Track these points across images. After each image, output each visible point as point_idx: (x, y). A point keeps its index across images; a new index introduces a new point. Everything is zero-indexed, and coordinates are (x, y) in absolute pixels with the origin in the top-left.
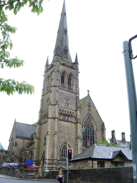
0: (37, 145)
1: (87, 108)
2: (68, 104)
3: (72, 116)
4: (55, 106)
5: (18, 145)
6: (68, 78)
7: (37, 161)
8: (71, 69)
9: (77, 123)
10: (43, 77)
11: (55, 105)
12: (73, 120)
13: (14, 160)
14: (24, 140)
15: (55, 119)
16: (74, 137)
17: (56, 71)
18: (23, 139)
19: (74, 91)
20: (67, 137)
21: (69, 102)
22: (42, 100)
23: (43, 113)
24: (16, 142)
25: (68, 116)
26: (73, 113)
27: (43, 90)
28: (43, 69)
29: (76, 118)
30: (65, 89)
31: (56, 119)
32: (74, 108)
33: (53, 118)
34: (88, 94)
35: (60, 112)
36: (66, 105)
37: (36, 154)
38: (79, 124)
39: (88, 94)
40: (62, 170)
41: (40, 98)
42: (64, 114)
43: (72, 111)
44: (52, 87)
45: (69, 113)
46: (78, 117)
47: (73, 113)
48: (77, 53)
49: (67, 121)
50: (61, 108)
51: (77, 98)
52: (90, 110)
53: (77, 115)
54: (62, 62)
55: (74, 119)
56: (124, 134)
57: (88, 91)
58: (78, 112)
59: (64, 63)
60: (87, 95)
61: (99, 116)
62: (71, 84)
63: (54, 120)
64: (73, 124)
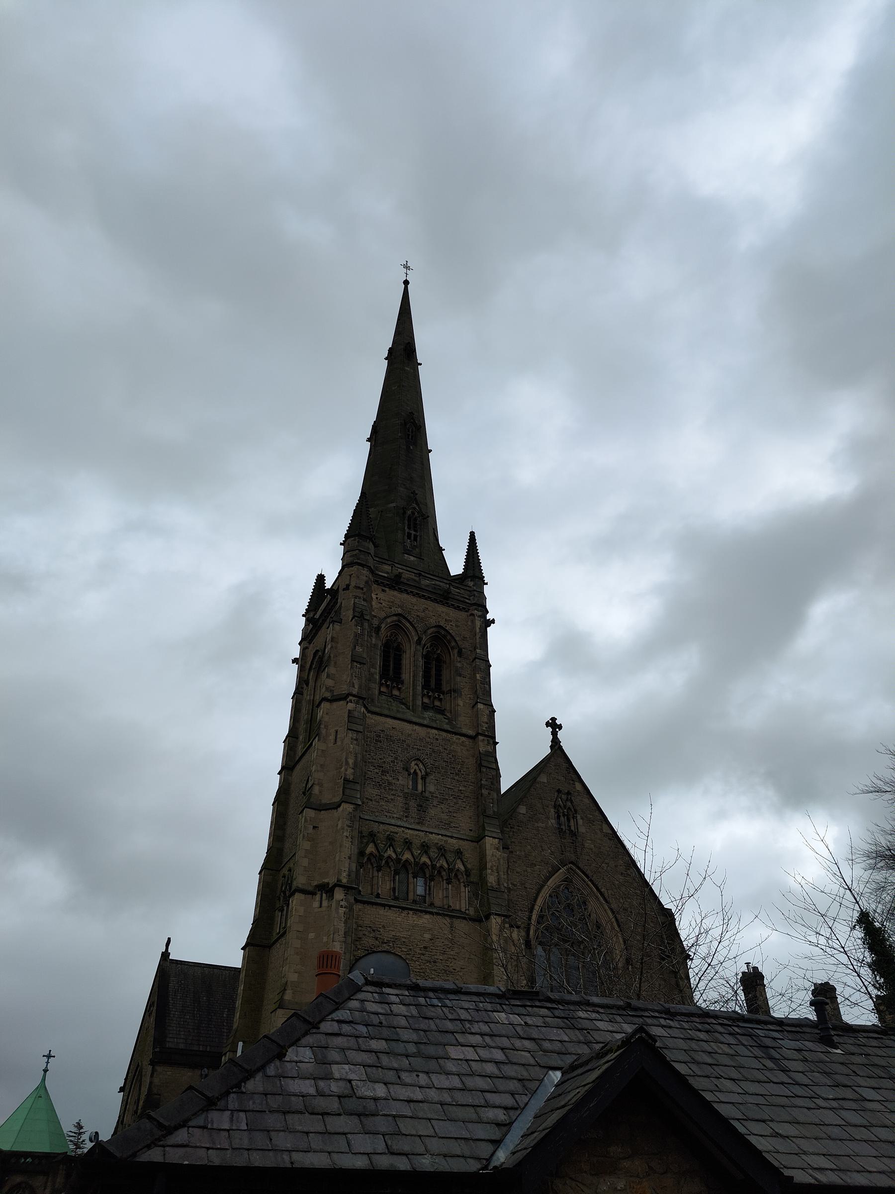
1: (552, 822)
3: (452, 876)
6: (426, 657)
8: (441, 609)
9: (487, 917)
10: (295, 666)
12: (462, 899)
17: (350, 614)
19: (464, 724)
21: (431, 788)
25: (429, 873)
30: (409, 715)
31: (339, 894)
32: (465, 822)
34: (556, 744)
35: (371, 848)
36: (413, 804)
38: (495, 922)
39: (556, 744)
42: (398, 860)
44: (325, 705)
45: (433, 853)
46: (492, 879)
49: (422, 906)
50: (375, 827)
52: (574, 834)
53: (482, 867)
54: (387, 568)
55: (465, 892)
57: (554, 725)
58: (490, 843)
59: (399, 576)
60: (545, 750)
62: (445, 688)
64: (462, 926)
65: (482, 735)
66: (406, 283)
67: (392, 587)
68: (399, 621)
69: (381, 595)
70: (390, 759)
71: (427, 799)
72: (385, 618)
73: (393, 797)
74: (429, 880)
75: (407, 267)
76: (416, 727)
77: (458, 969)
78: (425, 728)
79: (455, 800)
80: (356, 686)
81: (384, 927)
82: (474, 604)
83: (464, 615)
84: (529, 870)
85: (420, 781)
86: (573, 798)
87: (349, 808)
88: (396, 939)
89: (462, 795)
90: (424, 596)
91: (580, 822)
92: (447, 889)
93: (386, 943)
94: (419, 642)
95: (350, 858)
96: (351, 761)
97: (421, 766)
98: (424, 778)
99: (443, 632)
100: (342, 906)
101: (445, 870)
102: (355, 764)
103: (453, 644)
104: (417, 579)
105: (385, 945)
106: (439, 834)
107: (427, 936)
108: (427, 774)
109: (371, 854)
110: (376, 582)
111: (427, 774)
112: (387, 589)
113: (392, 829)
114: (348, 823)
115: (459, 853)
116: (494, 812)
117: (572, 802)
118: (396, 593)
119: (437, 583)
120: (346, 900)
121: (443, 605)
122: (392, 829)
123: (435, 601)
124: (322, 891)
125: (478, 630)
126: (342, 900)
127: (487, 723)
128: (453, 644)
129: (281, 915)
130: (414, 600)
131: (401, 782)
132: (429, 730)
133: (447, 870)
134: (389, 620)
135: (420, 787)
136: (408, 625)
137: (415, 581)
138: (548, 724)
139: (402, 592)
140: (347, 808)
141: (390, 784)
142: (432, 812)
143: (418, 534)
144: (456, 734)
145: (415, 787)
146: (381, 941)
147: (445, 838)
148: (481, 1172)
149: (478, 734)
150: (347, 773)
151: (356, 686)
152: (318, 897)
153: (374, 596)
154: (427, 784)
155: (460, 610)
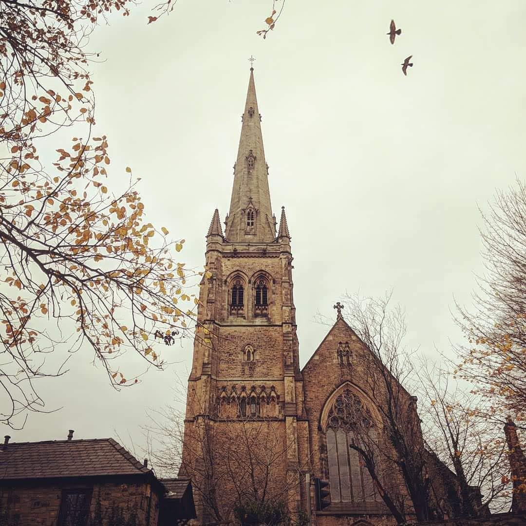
8: (263, 260)
36: (246, 367)
50: (225, 384)
65: (284, 323)
66: (252, 69)
67: (233, 257)
68: (238, 274)
69: (228, 263)
70: (233, 347)
71: (255, 363)
72: (230, 274)
73: (235, 367)
75: (252, 60)
76: (248, 328)
78: (253, 327)
79: (271, 361)
80: (209, 315)
82: (282, 252)
83: (277, 260)
84: (320, 389)
86: (350, 345)
87: (204, 378)
89: (275, 358)
90: (252, 256)
94: (250, 282)
96: (207, 354)
97: (251, 347)
98: (253, 353)
99: (264, 273)
102: (209, 355)
103: (270, 277)
104: (247, 248)
106: (261, 380)
108: (255, 351)
109: (224, 397)
110: (224, 257)
111: (255, 351)
112: (520, 277)
113: (235, 383)
115: (273, 388)
116: (291, 363)
117: (348, 347)
118: (235, 259)
119: (260, 247)
121: (264, 258)
122: (235, 383)
123: (258, 257)
125: (283, 266)
127: (288, 316)
128: (270, 277)
130: (246, 260)
131: (240, 358)
132: (255, 327)
134: (232, 275)
135: (252, 358)
136: (243, 274)
137: (246, 249)
138: (335, 307)
139: (239, 258)
141: (233, 360)
142: (257, 369)
143: (254, 221)
144: (271, 326)
145: (249, 359)
147: (265, 382)
149: (283, 323)
151: (209, 315)
153: (223, 265)
155: (274, 258)
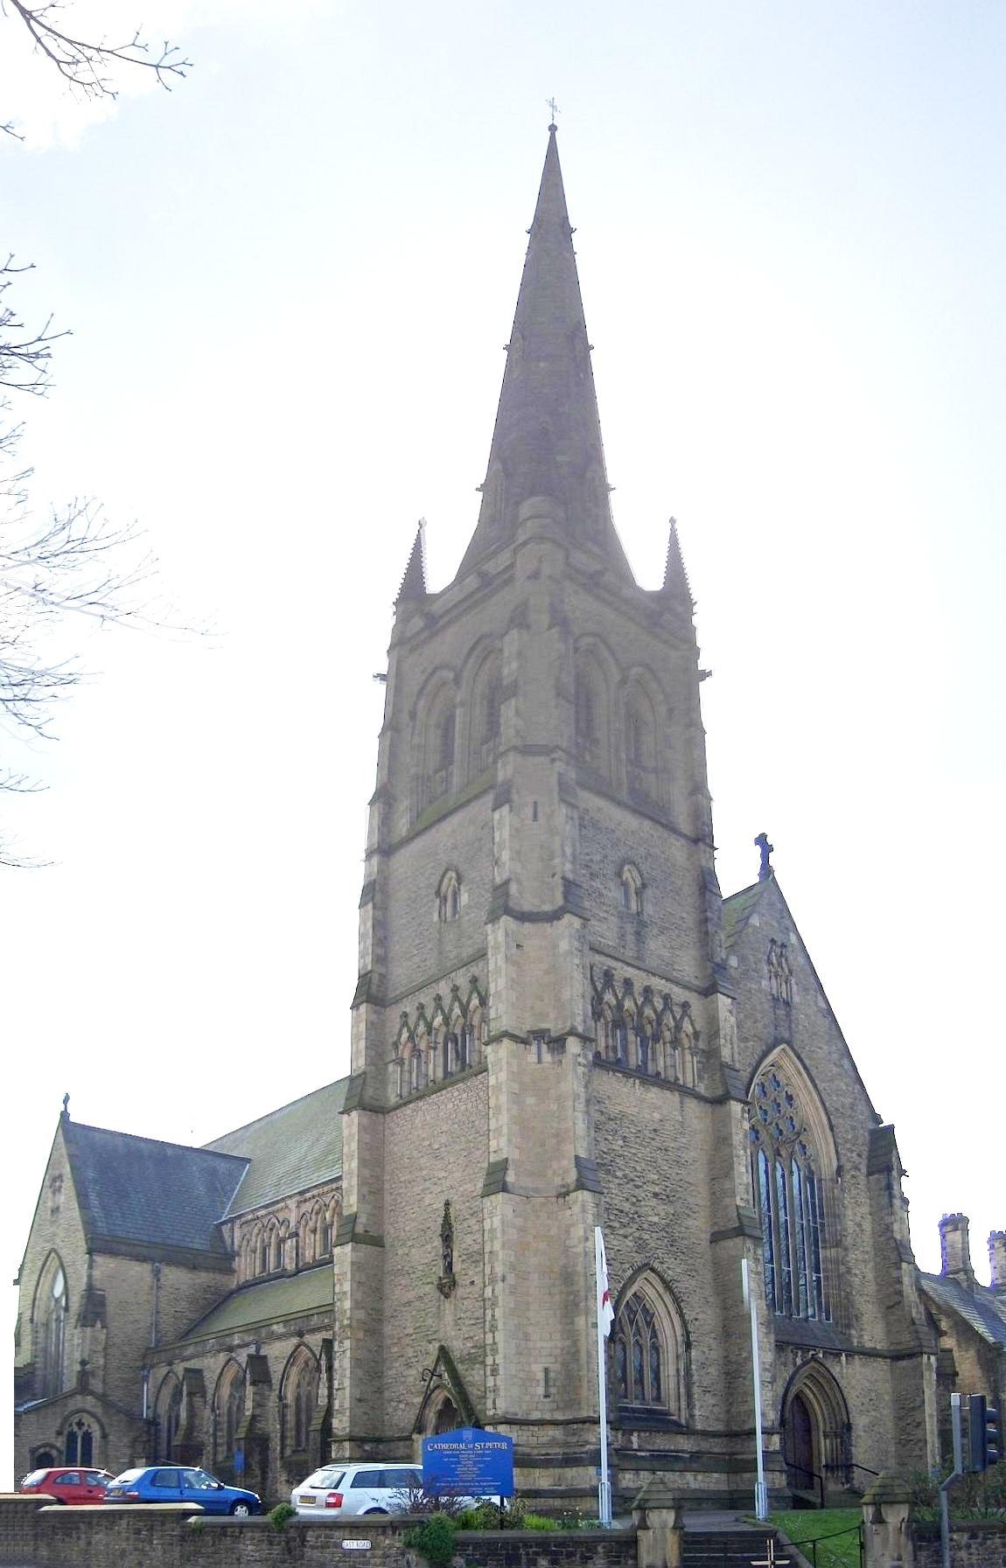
0: (359, 1296)
2: (640, 925)
4: (546, 927)
5: (111, 1309)
7: (363, 1440)
10: (381, 688)
11: (554, 916)
13: (96, 1434)
14: (157, 1273)
15: (557, 1044)
16: (698, 1226)
18: (147, 1267)
20: (655, 1213)
21: (649, 909)
22: (375, 894)
23: (394, 1014)
24: (90, 1288)
26: (685, 1006)
27: (384, 798)
28: (381, 624)
29: (710, 1055)
31: (573, 1045)
32: (688, 965)
33: (539, 1035)
34: (766, 870)
36: (630, 928)
37: (357, 1382)
39: (766, 870)
40: (911, 1520)
41: (354, 873)
43: (679, 994)
45: (658, 1003)
47: (685, 1006)
48: (672, 521)
51: (707, 882)
52: (787, 1004)
53: (714, 1034)
56: (966, 1232)
57: (766, 848)
61: (846, 1062)
63: (547, 1057)
64: (692, 1105)
73: (605, 915)
74: (653, 1040)
77: (690, 1161)
81: (609, 1097)
85: (633, 897)
88: (623, 1115)
91: (795, 988)
92: (673, 1056)
93: (612, 1120)
95: (583, 997)
96: (568, 851)
100: (580, 1064)
101: (669, 1030)
105: (611, 1123)
107: (657, 1116)
111: (644, 886)
114: (576, 944)
120: (585, 1057)
124: (539, 1041)
126: (579, 1055)
129: (401, 1071)
133: (673, 1030)
135: (634, 906)
140: (570, 922)
146: (607, 1116)
148: (446, 1460)
150: (566, 869)
152: (534, 1048)
154: (645, 903)
